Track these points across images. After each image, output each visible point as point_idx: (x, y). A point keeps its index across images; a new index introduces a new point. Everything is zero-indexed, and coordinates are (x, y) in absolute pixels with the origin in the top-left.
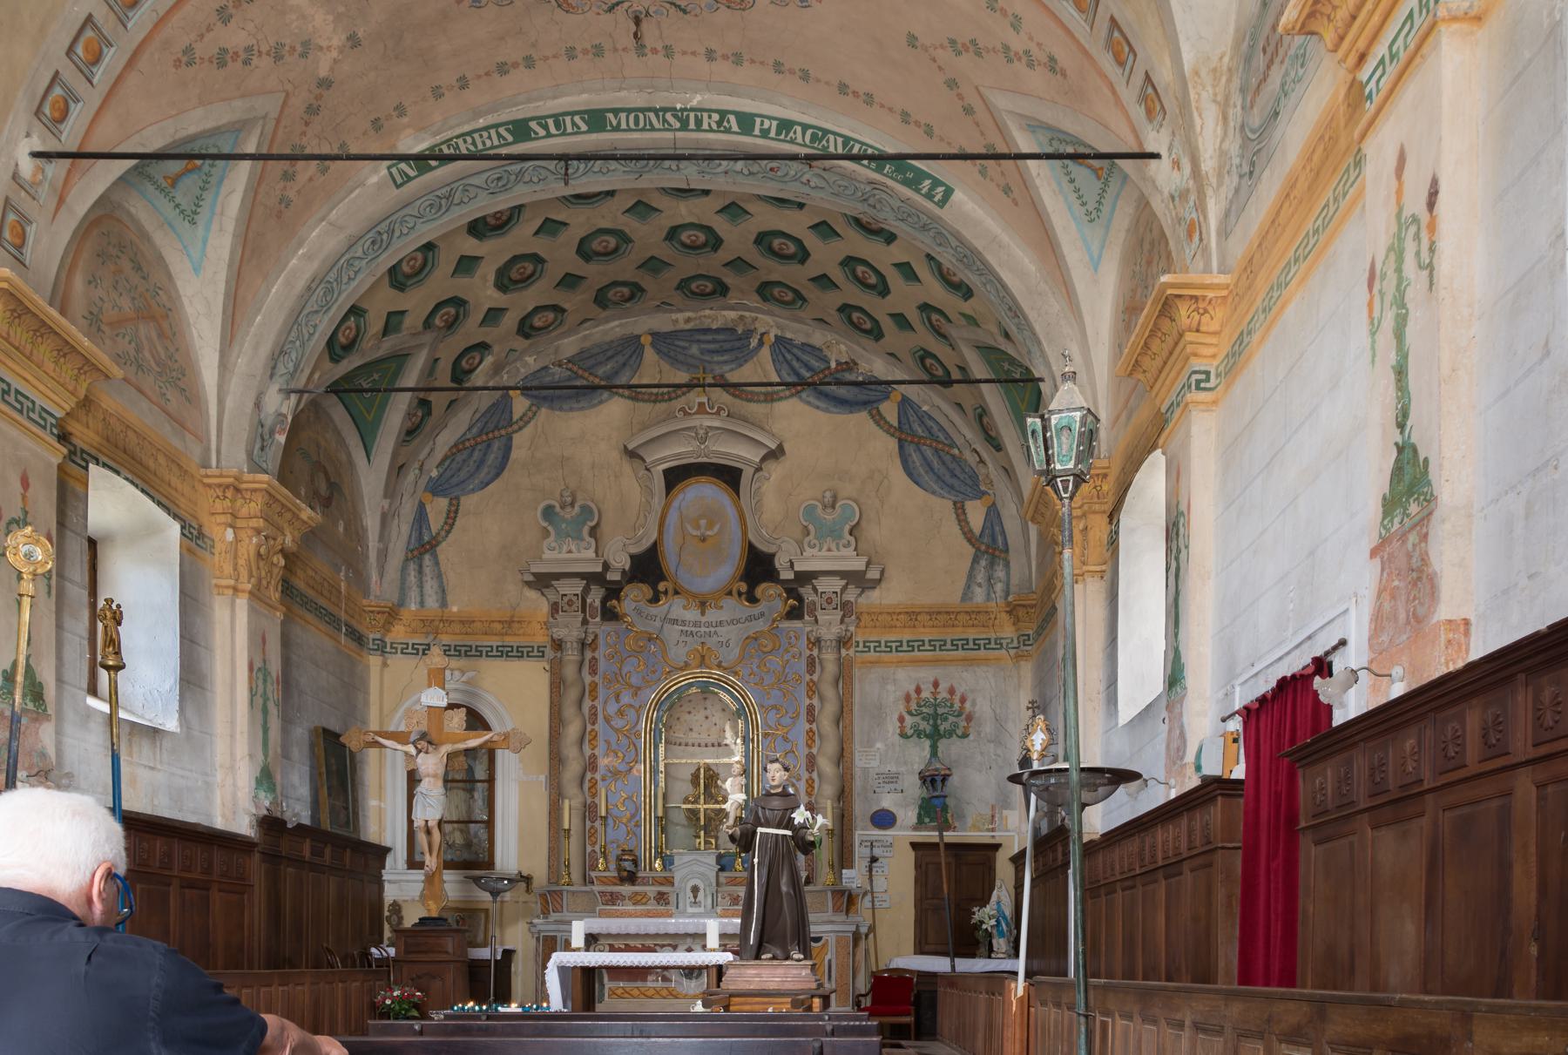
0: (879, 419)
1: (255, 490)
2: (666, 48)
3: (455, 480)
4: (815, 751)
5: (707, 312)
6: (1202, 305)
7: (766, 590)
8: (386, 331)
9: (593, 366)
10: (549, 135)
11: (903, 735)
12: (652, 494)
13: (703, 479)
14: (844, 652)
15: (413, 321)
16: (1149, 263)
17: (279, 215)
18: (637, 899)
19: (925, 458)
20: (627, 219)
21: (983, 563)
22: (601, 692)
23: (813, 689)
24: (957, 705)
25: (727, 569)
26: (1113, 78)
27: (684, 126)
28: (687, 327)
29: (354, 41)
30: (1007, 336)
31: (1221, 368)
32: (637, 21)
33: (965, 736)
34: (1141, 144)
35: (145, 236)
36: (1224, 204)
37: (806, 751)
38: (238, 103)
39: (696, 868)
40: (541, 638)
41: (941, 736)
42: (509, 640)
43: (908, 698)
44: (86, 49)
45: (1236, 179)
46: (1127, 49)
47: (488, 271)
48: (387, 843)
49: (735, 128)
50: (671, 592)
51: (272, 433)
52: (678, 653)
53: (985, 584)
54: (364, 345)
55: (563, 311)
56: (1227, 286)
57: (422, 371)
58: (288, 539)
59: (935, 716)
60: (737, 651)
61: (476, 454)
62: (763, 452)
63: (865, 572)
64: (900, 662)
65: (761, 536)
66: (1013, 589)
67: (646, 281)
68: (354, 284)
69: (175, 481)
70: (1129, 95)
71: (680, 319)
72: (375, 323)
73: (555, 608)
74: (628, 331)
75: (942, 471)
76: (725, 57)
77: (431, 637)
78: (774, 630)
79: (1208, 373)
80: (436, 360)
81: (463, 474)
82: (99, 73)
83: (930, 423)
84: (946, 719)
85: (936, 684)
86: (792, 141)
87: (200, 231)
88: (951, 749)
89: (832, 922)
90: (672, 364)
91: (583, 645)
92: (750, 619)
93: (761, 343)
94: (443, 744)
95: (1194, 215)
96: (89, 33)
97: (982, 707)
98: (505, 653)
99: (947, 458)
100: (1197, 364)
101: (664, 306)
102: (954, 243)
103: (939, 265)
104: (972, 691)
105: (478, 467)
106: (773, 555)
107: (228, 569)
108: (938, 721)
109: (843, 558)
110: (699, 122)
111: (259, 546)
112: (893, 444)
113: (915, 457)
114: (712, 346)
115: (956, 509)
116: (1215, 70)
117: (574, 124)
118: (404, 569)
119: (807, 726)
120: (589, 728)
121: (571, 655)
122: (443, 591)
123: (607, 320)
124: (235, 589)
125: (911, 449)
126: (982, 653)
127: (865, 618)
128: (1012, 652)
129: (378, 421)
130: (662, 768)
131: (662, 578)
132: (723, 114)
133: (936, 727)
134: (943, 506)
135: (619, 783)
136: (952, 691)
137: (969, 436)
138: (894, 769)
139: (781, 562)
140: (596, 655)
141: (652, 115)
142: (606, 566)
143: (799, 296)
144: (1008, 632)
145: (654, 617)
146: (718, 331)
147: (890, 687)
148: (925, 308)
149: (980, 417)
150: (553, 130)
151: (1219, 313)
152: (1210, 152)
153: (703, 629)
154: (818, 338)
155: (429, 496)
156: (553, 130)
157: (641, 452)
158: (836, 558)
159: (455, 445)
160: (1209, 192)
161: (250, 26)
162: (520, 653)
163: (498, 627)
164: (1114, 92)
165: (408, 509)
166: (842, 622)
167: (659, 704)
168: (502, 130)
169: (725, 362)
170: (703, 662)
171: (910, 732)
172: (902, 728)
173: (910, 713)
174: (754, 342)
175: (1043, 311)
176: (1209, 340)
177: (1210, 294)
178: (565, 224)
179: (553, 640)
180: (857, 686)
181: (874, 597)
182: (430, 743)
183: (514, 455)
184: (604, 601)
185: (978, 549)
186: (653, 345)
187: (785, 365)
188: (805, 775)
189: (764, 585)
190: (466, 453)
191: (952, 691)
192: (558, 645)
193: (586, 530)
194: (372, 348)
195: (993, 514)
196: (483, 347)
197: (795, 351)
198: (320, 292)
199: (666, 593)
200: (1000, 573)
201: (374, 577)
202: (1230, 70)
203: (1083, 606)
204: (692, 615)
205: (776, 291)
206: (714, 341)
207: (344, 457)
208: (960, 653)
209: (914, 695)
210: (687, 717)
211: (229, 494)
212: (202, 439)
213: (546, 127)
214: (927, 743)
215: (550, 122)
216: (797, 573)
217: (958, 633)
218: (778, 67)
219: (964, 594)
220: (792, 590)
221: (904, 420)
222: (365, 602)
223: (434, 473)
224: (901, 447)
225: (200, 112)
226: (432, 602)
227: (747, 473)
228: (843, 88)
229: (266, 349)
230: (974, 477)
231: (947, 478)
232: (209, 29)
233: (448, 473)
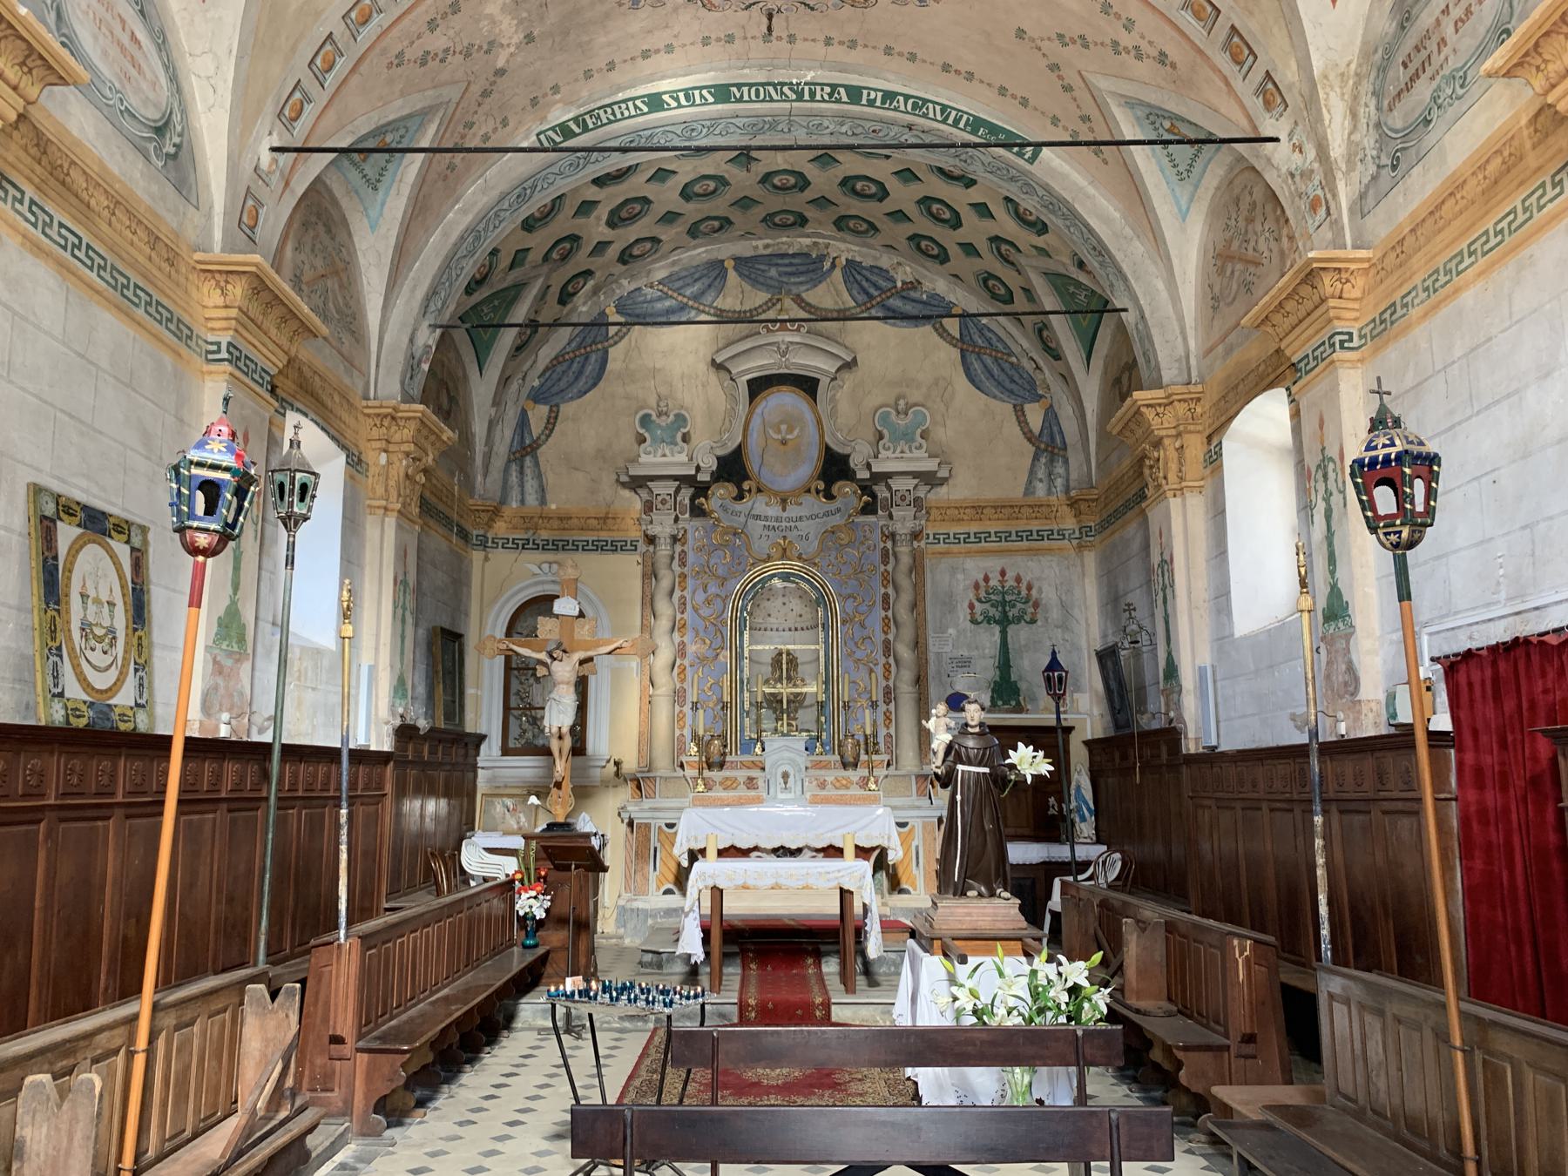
0: (943, 333)
1: (409, 418)
2: (790, 36)
3: (555, 390)
4: (891, 637)
6: (1344, 275)
7: (845, 489)
8: (512, 267)
10: (680, 106)
11: (974, 621)
12: (737, 402)
13: (784, 388)
14: (916, 544)
15: (535, 257)
16: (1250, 220)
17: (446, 178)
18: (729, 785)
20: (729, 167)
21: (1043, 460)
22: (690, 582)
24: (1024, 592)
25: (807, 468)
26: (1227, 72)
27: (800, 98)
29: (529, 38)
30: (1081, 265)
31: (1366, 330)
32: (770, 17)
33: (1033, 621)
34: (1255, 128)
35: (335, 202)
36: (1356, 189)
37: (883, 637)
38: (430, 93)
39: (787, 754)
42: (604, 535)
43: (977, 586)
44: (324, 60)
45: (1372, 169)
46: (1246, 52)
47: (603, 212)
48: (482, 730)
49: (845, 99)
50: (754, 490)
51: (419, 365)
52: (761, 546)
55: (659, 241)
56: (1369, 260)
58: (431, 457)
62: (839, 363)
64: (968, 553)
66: (1072, 484)
67: (736, 215)
69: (345, 416)
70: (1246, 88)
71: (758, 246)
72: (505, 260)
73: (648, 507)
75: (1002, 377)
76: (841, 43)
78: (851, 526)
79: (1350, 334)
81: (563, 384)
82: (330, 77)
85: (1003, 573)
86: (896, 109)
87: (381, 193)
88: (1019, 634)
91: (675, 539)
92: (827, 514)
93: (833, 266)
94: (573, 651)
95: (1319, 192)
96: (328, 47)
97: (1049, 595)
98: (599, 547)
99: (1006, 366)
100: (1340, 326)
101: (748, 235)
102: (1041, 192)
103: (1016, 205)
104: (1038, 579)
105: (577, 379)
107: (380, 490)
108: (1006, 609)
109: (918, 459)
110: (812, 94)
111: (408, 467)
112: (955, 354)
113: (977, 365)
114: (789, 269)
116: (1342, 75)
117: (702, 96)
118: (506, 470)
119: (883, 614)
120: (679, 616)
121: (664, 550)
122: (542, 490)
123: (695, 247)
124: (386, 509)
125: (972, 358)
126: (1046, 543)
127: (934, 512)
128: (1075, 542)
129: (488, 346)
130: (746, 654)
131: (747, 477)
132: (834, 87)
133: (1005, 613)
134: (1004, 409)
136: (1018, 579)
137: (1026, 345)
138: (966, 654)
139: (856, 462)
141: (771, 89)
142: (698, 469)
143: (872, 226)
144: (1070, 523)
145: (738, 514)
146: (794, 255)
147: (960, 576)
148: (995, 239)
149: (1040, 331)
150: (683, 102)
151: (1360, 282)
152: (1339, 141)
154: (886, 261)
155: (531, 403)
156: (683, 102)
157: (727, 365)
158: (911, 459)
159: (556, 358)
160: (1339, 175)
161: (451, 33)
162: (615, 547)
163: (595, 522)
164: (1228, 84)
165: (511, 415)
167: (743, 594)
168: (638, 103)
172: (972, 614)
173: (979, 600)
174: (827, 265)
175: (1130, 252)
176: (1351, 305)
177: (1353, 266)
178: (674, 172)
179: (646, 536)
180: (928, 576)
183: (610, 366)
184: (692, 500)
185: (1038, 448)
186: (735, 268)
188: (883, 660)
189: (839, 483)
190: (565, 365)
191: (1018, 579)
192: (651, 540)
193: (679, 436)
194: (499, 282)
195: (1051, 416)
196: (588, 273)
198: (470, 239)
200: (1059, 469)
201: (479, 478)
202: (1357, 74)
203: (1182, 519)
204: (774, 511)
205: (851, 224)
206: (791, 264)
207: (460, 374)
208: (1025, 544)
209: (982, 584)
210: (766, 604)
211: (386, 423)
212: (366, 375)
213: (677, 99)
214: (997, 629)
215: (681, 95)
217: (1022, 525)
218: (888, 51)
220: (866, 488)
222: (471, 502)
223: (536, 383)
224: (963, 357)
225: (400, 102)
226: (532, 500)
227: (824, 381)
228: (946, 68)
229: (420, 294)
230: (1032, 382)
231: (1007, 384)
232: (419, 37)
233: (549, 384)
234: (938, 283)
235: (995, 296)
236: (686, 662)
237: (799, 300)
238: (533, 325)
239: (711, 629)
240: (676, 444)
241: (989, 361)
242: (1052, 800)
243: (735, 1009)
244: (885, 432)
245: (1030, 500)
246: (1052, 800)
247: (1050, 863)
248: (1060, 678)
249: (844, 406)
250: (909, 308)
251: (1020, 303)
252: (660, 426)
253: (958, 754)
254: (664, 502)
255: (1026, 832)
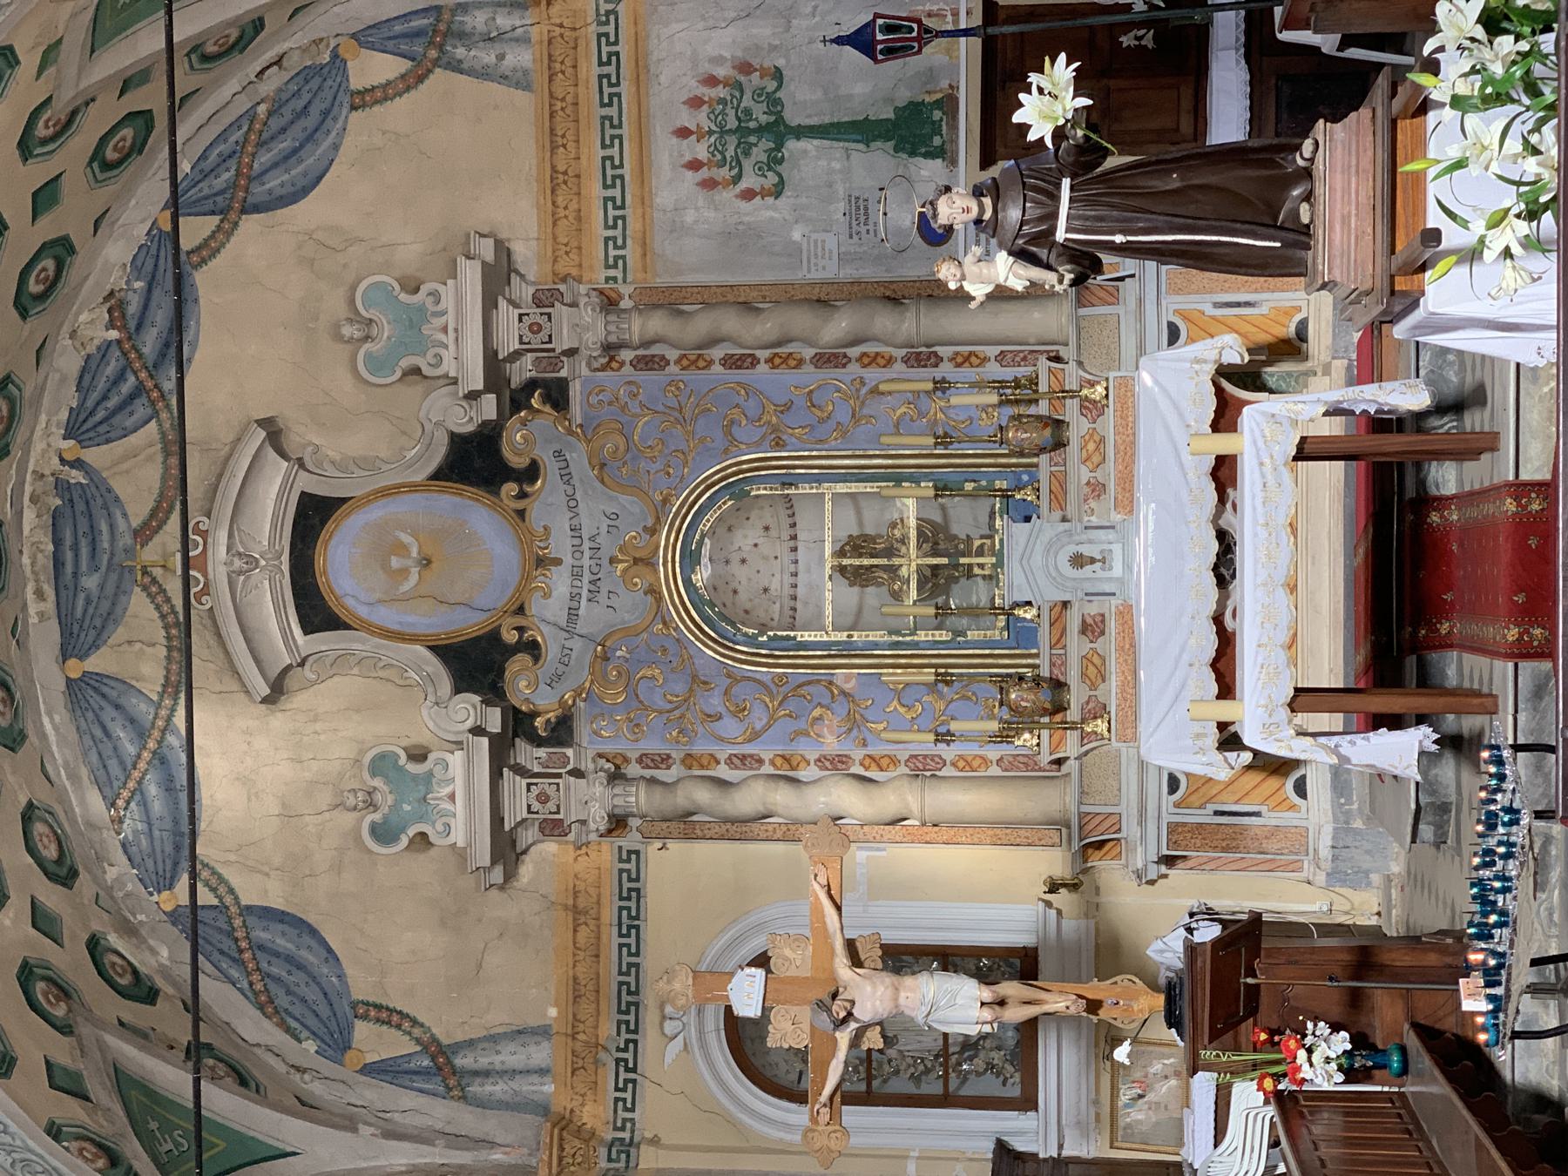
0: (208, 249)
3: (324, 1011)
4: (808, 353)
5: (26, 560)
7: (516, 443)
9: (122, 763)
11: (778, 191)
13: (319, 562)
14: (626, 303)
15: (62, 1051)
18: (1095, 672)
19: (275, 165)
21: (460, 52)
22: (701, 747)
23: (695, 359)
25: (475, 517)
28: (49, 591)
33: (778, 75)
37: (809, 368)
40: (605, 854)
41: (780, 120)
42: (609, 914)
43: (709, 184)
50: (519, 621)
52: (628, 606)
53: (498, 48)
54: (103, 1132)
55: (30, 805)
57: (141, 1048)
59: (742, 132)
60: (624, 499)
61: (274, 970)
62: (271, 453)
63: (484, 264)
64: (644, 201)
65: (419, 457)
68: (13, 1127)
72: (70, 1110)
73: (554, 828)
74: (60, 700)
75: (297, 132)
77: (602, 1055)
78: (588, 432)
80: (121, 1024)
81: (312, 994)
83: (213, 156)
84: (748, 112)
85: (683, 133)
89: (1141, 302)
90: (117, 623)
91: (616, 777)
92: (566, 477)
93: (78, 464)
98: (631, 925)
99: (275, 124)
106: (453, 437)
112: (250, 224)
113: (274, 182)
114: (84, 551)
115: (364, 106)
118: (482, 1104)
119: (763, 368)
121: (637, 798)
123: (43, 736)
125: (259, 192)
126: (624, 48)
127: (562, 268)
129: (238, 1140)
130: (842, 636)
131: (494, 636)
133: (761, 130)
134: (360, 129)
135: (869, 715)
136: (695, 103)
137: (233, 86)
139: (464, 421)
140: (634, 756)
142: (478, 731)
146: (57, 542)
149: (206, 58)
153: (586, 562)
154: (67, 361)
155: (350, 1054)
157: (274, 673)
159: (261, 1008)
162: (632, 892)
163: (584, 934)
165: (375, 1094)
166: (574, 305)
167: (724, 642)
169: (112, 527)
170: (645, 562)
171: (772, 178)
172: (764, 193)
173: (737, 179)
174: (76, 476)
179: (610, 832)
181: (524, 252)
182: (834, 996)
183: (277, 903)
184: (539, 742)
185: (436, 63)
186: (82, 657)
187: (116, 420)
188: (854, 369)
189: (506, 452)
190: (272, 987)
191: (695, 103)
192: (618, 823)
194: (111, 1121)
196: (94, 945)
197: (90, 404)
199: (521, 629)
201: (497, 1156)
204: (560, 582)
206: (75, 548)
208: (625, 88)
209: (704, 173)
210: (743, 596)
214: (792, 145)
216: (488, 388)
217: (589, 94)
219: (517, 85)
220: (516, 401)
221: (209, 205)
223: (311, 1046)
224: (257, 209)
226: (539, 1054)
230: (307, 74)
231: (310, 122)
233: (312, 1021)
234: (111, 260)
235: (138, 147)
236: (858, 754)
237: (145, 533)
238: (196, 1053)
239: (792, 705)
240: (430, 774)
241: (265, 158)
242: (1127, 40)
243: (1527, 667)
244: (405, 363)
245: (540, 80)
246: (1127, 40)
247: (1247, 45)
248: (889, 29)
249: (355, 443)
250: (161, 316)
251: (152, 97)
252: (395, 807)
253: (1035, 239)
254: (543, 798)
255: (1187, 93)
